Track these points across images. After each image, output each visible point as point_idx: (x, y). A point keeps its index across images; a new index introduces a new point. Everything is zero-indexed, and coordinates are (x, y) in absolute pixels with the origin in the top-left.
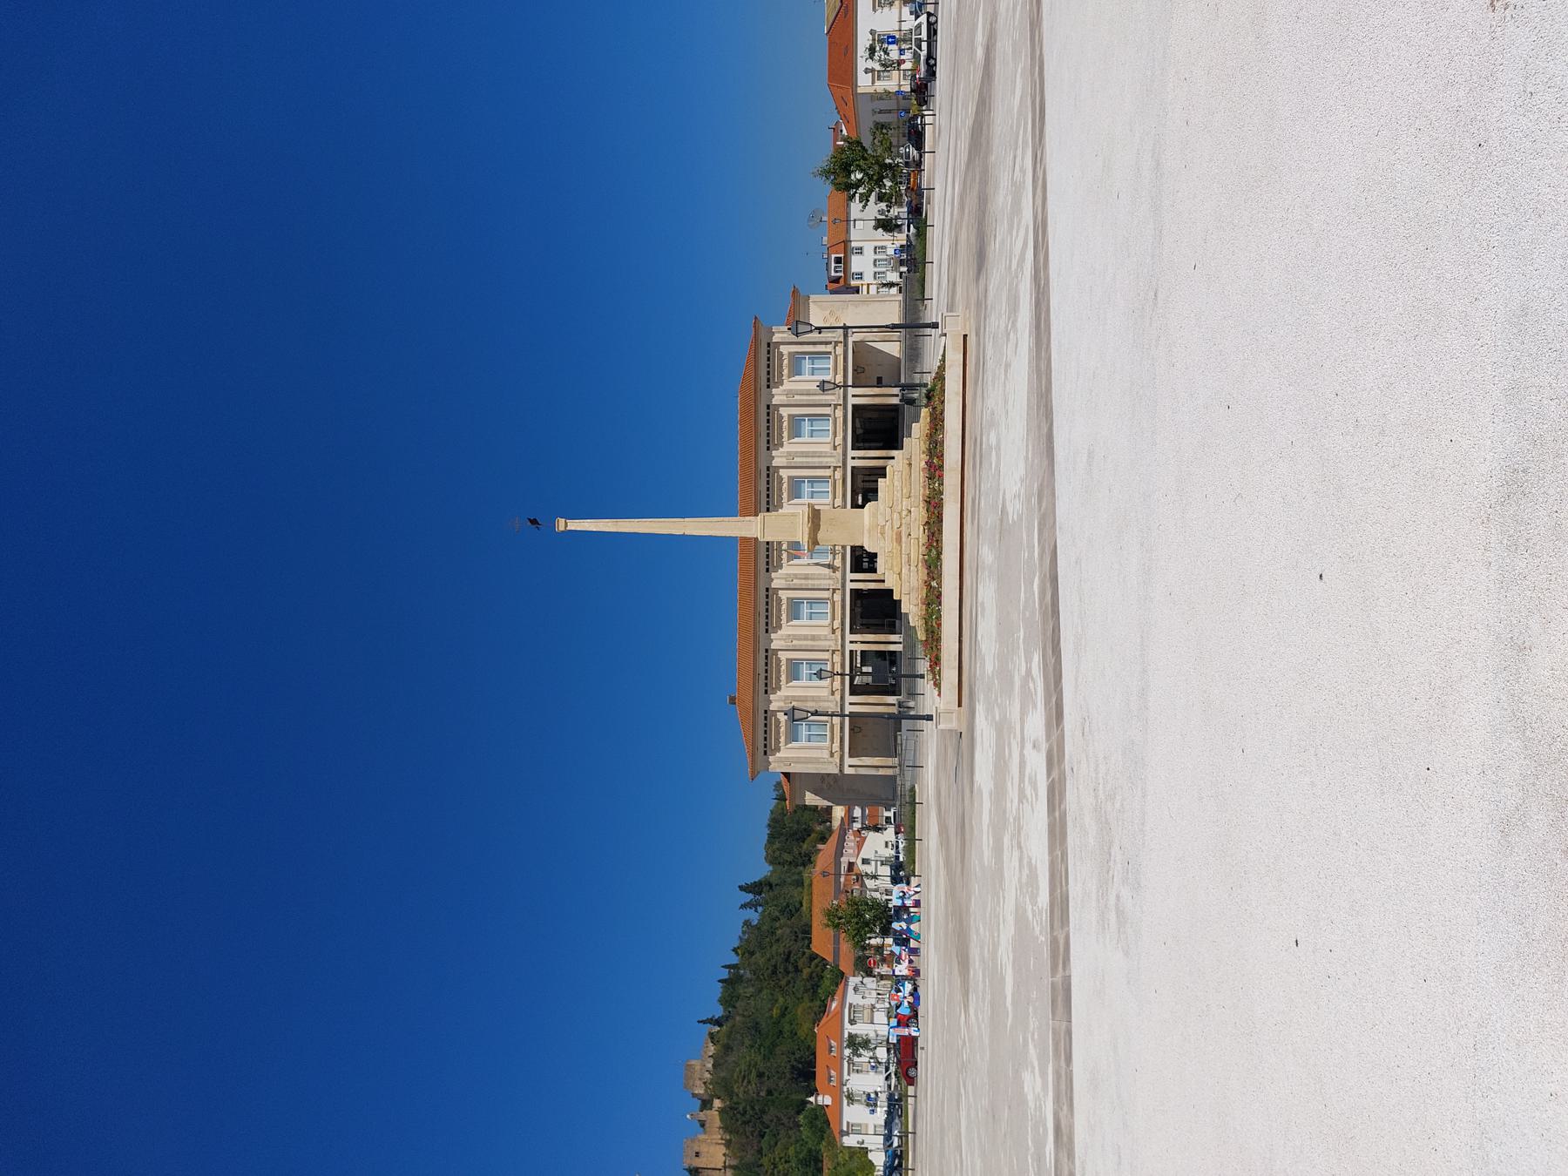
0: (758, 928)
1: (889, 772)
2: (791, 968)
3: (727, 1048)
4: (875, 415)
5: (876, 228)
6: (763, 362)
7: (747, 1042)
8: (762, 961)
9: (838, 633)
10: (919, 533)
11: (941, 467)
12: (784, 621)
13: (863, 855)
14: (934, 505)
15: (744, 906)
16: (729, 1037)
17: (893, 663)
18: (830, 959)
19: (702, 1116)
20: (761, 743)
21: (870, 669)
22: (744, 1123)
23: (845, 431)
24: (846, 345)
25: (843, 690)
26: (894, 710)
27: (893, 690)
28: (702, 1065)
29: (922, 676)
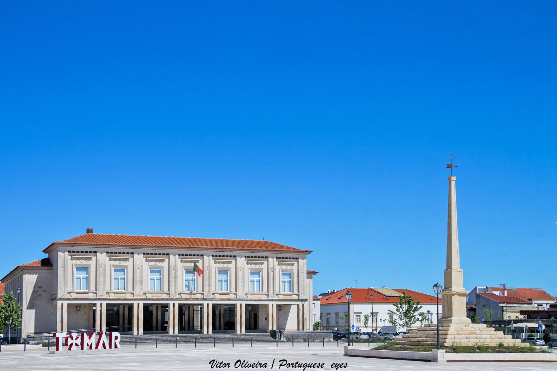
9: (144, 297)
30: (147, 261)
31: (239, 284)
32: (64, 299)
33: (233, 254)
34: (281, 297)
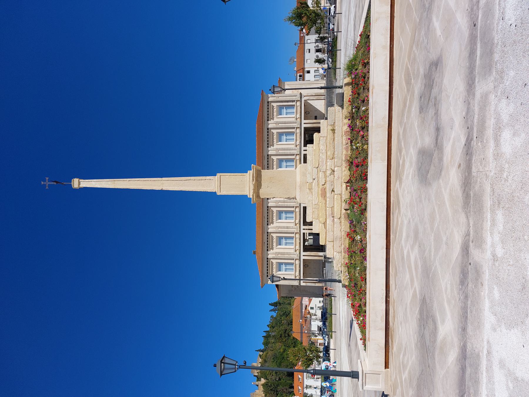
0: (275, 318)
2: (286, 335)
3: (265, 361)
9: (298, 225)
10: (343, 191)
13: (311, 306)
14: (358, 166)
15: (271, 311)
18: (299, 339)
19: (257, 383)
21: (312, 237)
23: (301, 139)
24: (301, 102)
25: (300, 250)
26: (323, 258)
30: (272, 249)
33: (266, 157)
34: (298, 116)
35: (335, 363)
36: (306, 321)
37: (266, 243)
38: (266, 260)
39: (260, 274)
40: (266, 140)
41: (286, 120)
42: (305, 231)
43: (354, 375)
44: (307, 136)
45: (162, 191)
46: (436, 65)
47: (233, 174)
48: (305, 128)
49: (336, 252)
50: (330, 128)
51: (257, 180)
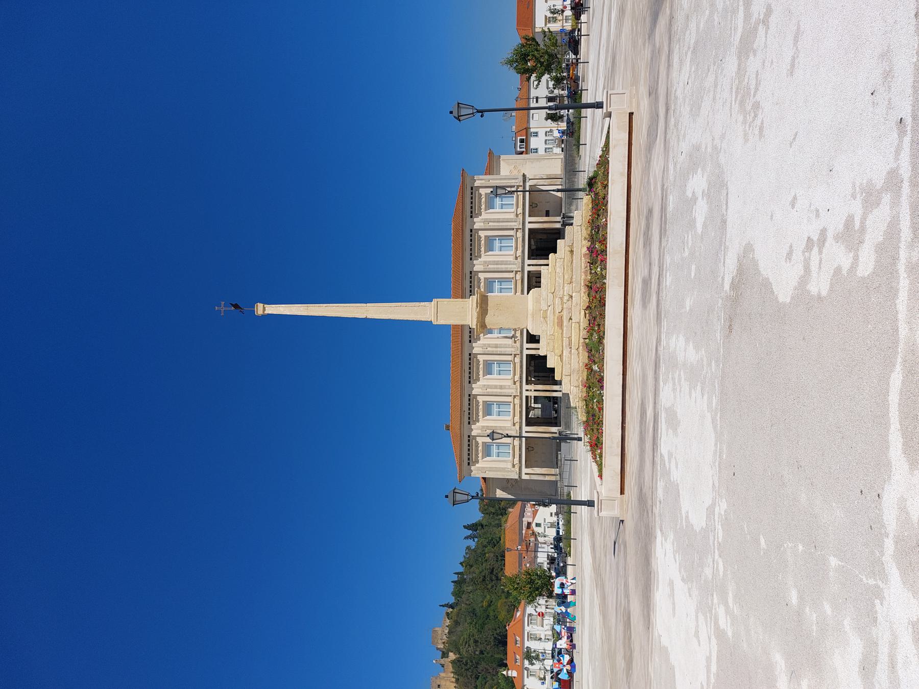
1: (553, 478)
2: (494, 578)
3: (457, 623)
4: (544, 237)
5: (546, 119)
6: (468, 201)
7: (469, 621)
8: (477, 571)
9: (518, 384)
10: (580, 318)
11: (604, 252)
12: (481, 376)
13: (536, 521)
14: (596, 292)
15: (466, 538)
16: (458, 616)
17: (555, 403)
20: (465, 457)
21: (540, 406)
22: (467, 670)
23: (523, 246)
25: (521, 423)
27: (555, 422)
28: (442, 630)
29: (580, 439)
31: (503, 267)
32: (520, 473)
34: (520, 210)
35: (574, 579)
36: (528, 546)
37: (467, 412)
38: (466, 439)
39: (457, 461)
40: (468, 248)
41: (502, 221)
42: (528, 394)
43: (590, 504)
44: (533, 243)
45: (366, 320)
46: (650, 212)
47: (417, 304)
48: (530, 230)
49: (571, 386)
50: (568, 249)
51: (481, 307)
